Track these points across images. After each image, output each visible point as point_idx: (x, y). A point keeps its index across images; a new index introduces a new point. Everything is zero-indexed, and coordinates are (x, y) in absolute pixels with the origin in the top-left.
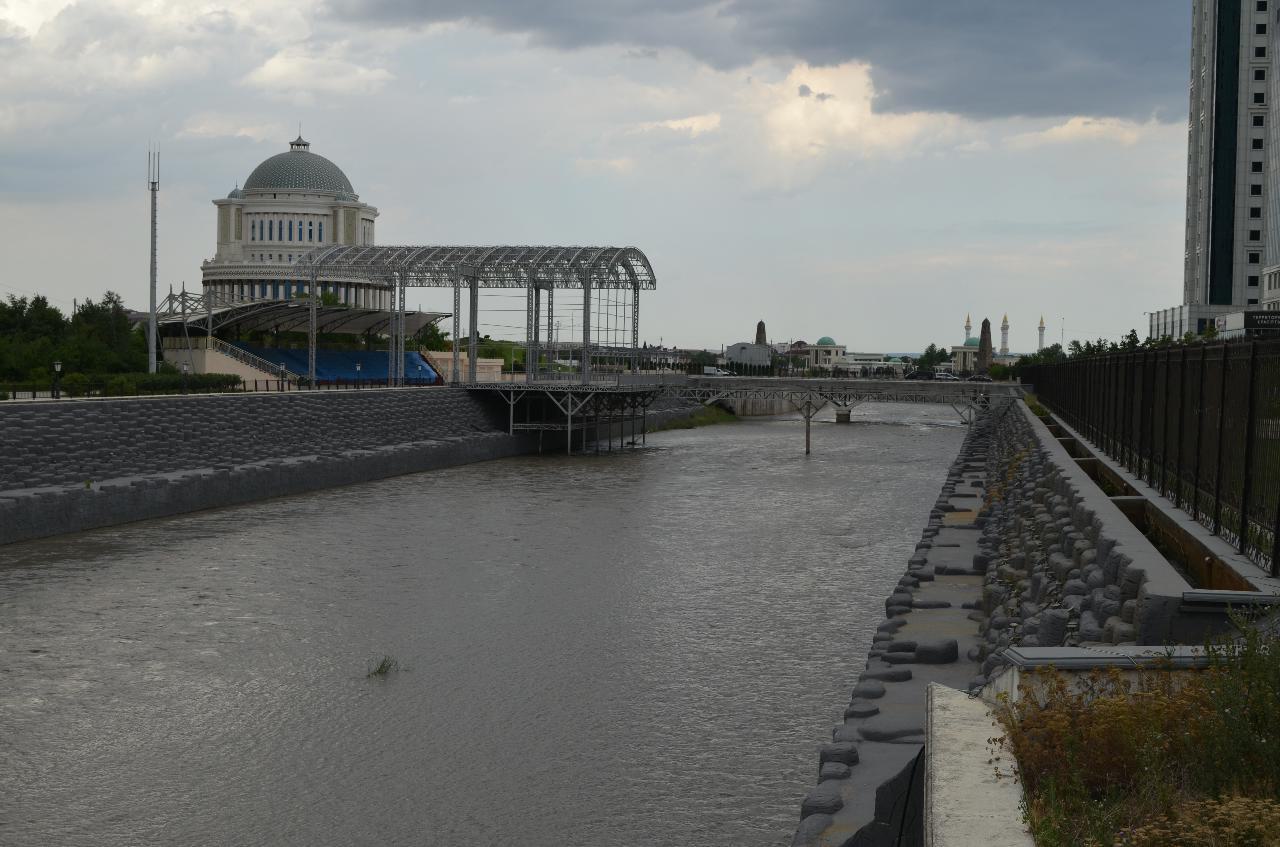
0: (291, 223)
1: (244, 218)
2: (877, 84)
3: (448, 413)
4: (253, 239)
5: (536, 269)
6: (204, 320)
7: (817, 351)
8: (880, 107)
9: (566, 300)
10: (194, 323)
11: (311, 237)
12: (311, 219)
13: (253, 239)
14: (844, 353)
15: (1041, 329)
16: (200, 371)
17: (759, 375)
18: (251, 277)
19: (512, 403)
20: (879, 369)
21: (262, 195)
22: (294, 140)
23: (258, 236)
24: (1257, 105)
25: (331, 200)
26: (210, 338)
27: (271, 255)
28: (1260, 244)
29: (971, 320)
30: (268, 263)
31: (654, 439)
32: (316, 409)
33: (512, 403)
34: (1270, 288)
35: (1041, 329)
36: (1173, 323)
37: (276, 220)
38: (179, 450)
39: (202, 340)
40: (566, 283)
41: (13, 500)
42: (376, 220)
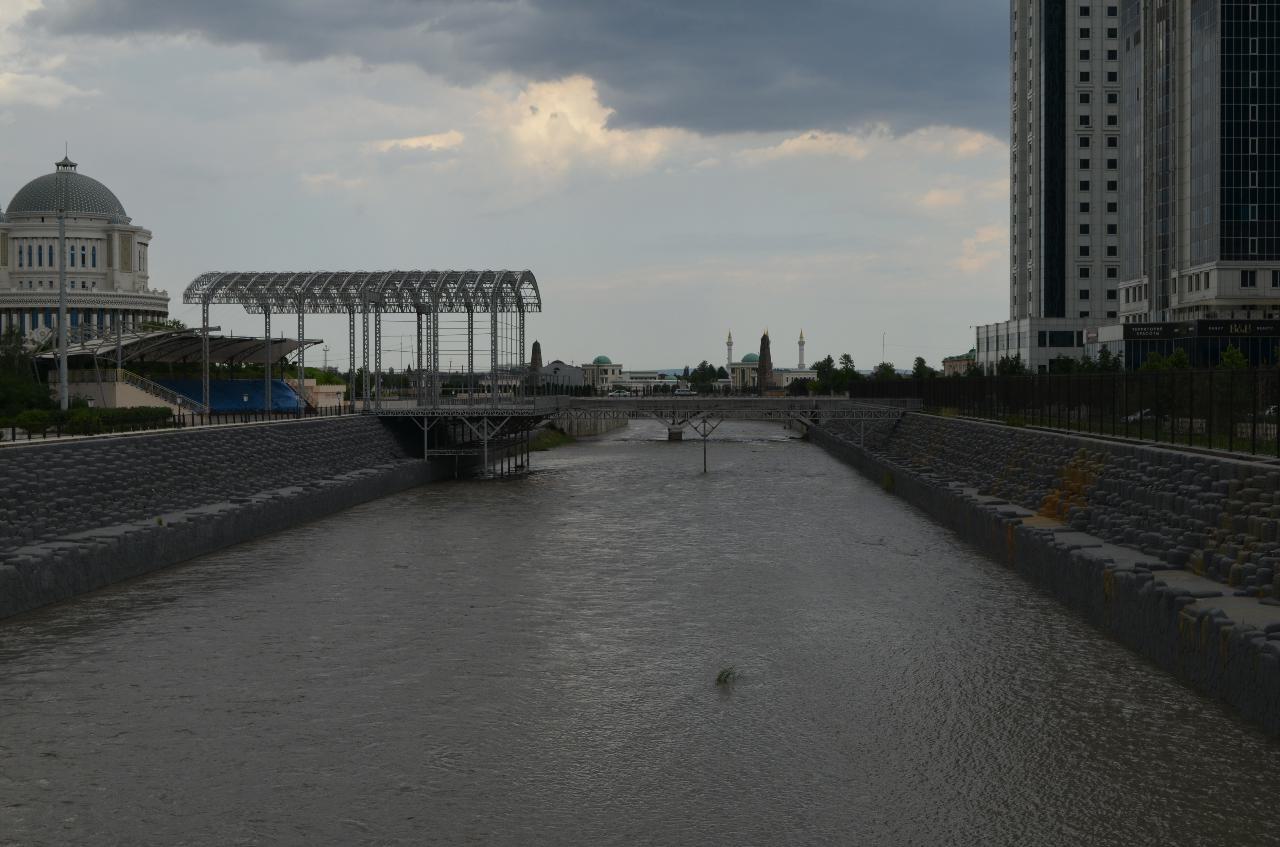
0: (51, 247)
1: (10, 242)
2: (604, 100)
3: (372, 441)
4: (21, 265)
5: (423, 293)
6: (114, 351)
7: (743, 371)
8: (612, 124)
9: (451, 323)
10: (103, 355)
11: (83, 262)
12: (84, 243)
13: (21, 265)
14: (620, 372)
15: (730, 344)
16: (110, 406)
17: (576, 395)
18: (20, 305)
19: (426, 429)
20: (656, 387)
21: (28, 218)
22: (60, 159)
23: (26, 261)
24: (1083, 127)
25: (104, 224)
26: (119, 369)
27: (41, 282)
28: (1118, 260)
29: (804, 336)
30: (40, 290)
31: (539, 461)
32: (281, 440)
33: (426, 429)
34: (1127, 301)
35: (730, 344)
36: (988, 338)
37: (35, 245)
38: (199, 485)
39: (110, 371)
40: (451, 307)
41: (115, 540)
42: (150, 243)
